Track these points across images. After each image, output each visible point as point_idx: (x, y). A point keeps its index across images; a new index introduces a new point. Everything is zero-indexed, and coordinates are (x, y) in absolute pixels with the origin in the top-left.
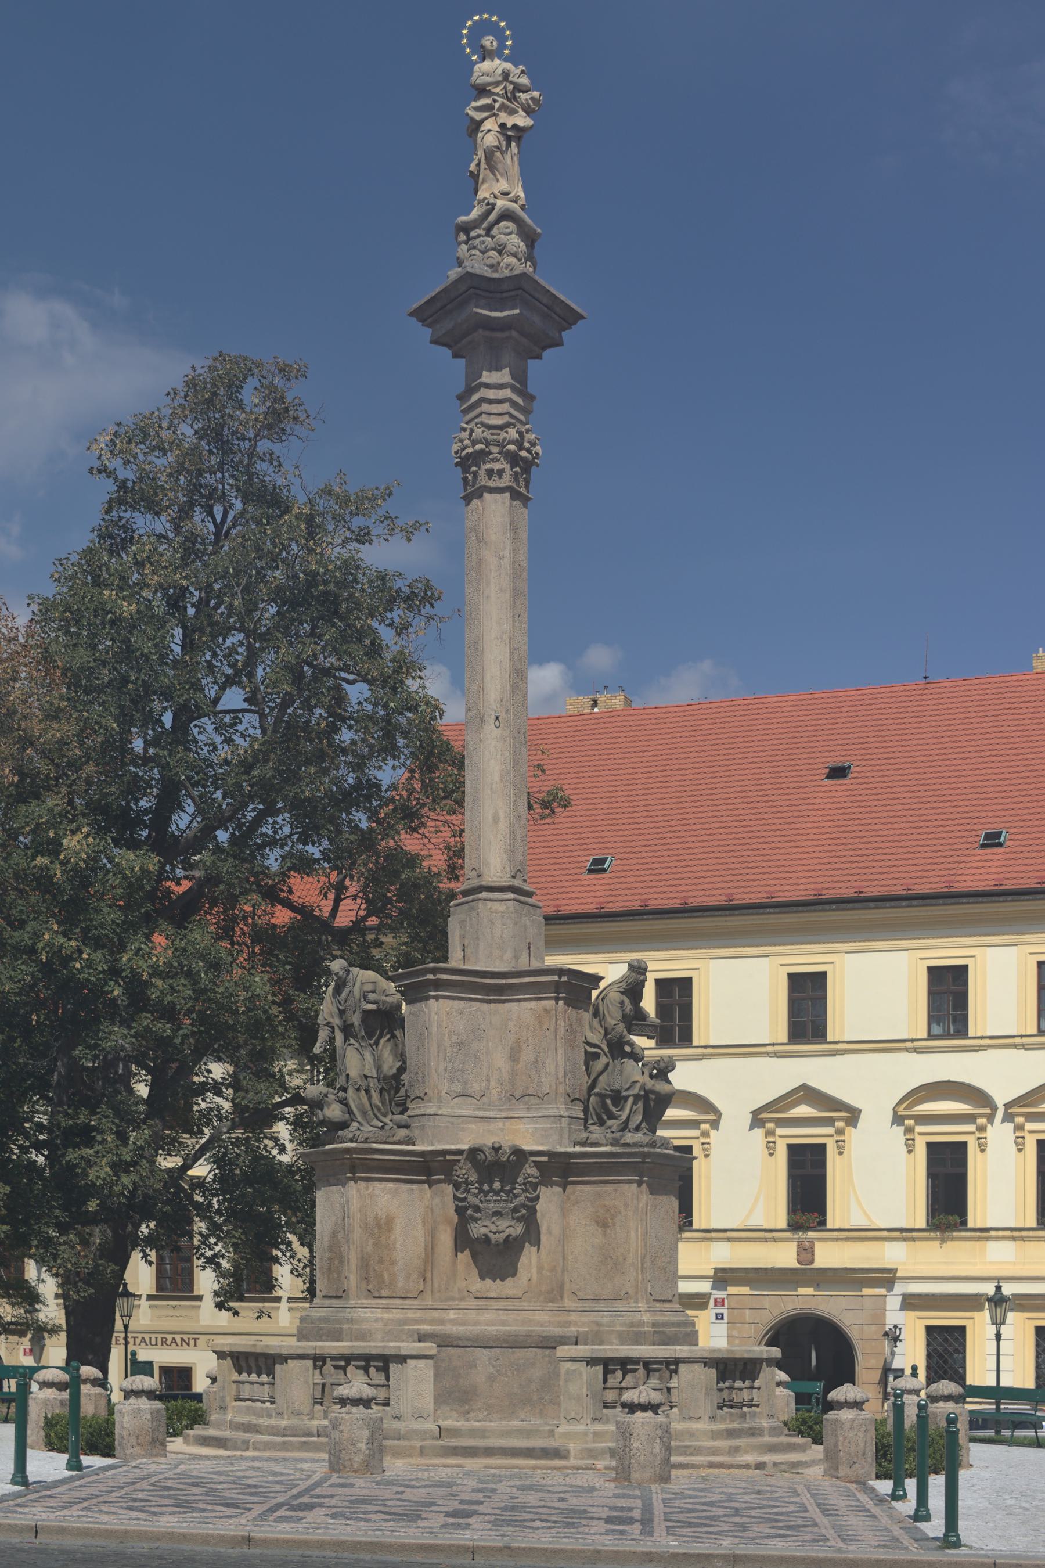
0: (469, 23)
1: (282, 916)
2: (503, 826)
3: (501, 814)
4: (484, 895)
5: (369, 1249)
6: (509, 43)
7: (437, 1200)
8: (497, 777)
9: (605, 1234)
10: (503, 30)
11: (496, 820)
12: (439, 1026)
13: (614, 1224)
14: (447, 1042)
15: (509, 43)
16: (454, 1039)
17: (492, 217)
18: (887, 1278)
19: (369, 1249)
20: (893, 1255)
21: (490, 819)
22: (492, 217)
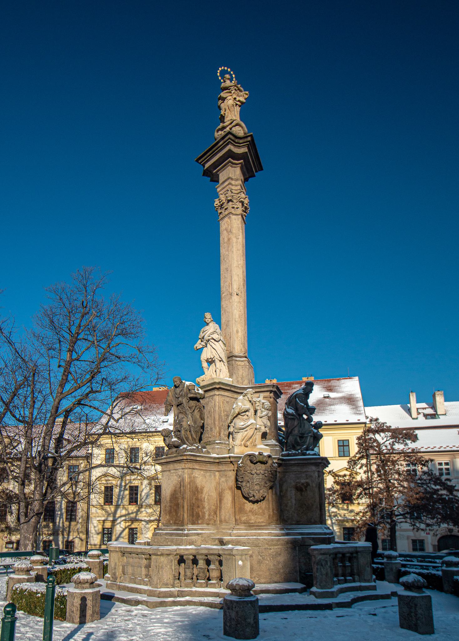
0: (218, 74)
1: (39, 595)
2: (240, 334)
3: (240, 330)
4: (234, 358)
5: (194, 501)
6: (229, 70)
7: (223, 479)
8: (237, 316)
9: (301, 495)
10: (230, 72)
11: (237, 332)
12: (219, 407)
13: (306, 490)
14: (223, 414)
15: (229, 70)
16: (225, 413)
17: (233, 124)
19: (194, 501)
21: (235, 332)
22: (233, 124)
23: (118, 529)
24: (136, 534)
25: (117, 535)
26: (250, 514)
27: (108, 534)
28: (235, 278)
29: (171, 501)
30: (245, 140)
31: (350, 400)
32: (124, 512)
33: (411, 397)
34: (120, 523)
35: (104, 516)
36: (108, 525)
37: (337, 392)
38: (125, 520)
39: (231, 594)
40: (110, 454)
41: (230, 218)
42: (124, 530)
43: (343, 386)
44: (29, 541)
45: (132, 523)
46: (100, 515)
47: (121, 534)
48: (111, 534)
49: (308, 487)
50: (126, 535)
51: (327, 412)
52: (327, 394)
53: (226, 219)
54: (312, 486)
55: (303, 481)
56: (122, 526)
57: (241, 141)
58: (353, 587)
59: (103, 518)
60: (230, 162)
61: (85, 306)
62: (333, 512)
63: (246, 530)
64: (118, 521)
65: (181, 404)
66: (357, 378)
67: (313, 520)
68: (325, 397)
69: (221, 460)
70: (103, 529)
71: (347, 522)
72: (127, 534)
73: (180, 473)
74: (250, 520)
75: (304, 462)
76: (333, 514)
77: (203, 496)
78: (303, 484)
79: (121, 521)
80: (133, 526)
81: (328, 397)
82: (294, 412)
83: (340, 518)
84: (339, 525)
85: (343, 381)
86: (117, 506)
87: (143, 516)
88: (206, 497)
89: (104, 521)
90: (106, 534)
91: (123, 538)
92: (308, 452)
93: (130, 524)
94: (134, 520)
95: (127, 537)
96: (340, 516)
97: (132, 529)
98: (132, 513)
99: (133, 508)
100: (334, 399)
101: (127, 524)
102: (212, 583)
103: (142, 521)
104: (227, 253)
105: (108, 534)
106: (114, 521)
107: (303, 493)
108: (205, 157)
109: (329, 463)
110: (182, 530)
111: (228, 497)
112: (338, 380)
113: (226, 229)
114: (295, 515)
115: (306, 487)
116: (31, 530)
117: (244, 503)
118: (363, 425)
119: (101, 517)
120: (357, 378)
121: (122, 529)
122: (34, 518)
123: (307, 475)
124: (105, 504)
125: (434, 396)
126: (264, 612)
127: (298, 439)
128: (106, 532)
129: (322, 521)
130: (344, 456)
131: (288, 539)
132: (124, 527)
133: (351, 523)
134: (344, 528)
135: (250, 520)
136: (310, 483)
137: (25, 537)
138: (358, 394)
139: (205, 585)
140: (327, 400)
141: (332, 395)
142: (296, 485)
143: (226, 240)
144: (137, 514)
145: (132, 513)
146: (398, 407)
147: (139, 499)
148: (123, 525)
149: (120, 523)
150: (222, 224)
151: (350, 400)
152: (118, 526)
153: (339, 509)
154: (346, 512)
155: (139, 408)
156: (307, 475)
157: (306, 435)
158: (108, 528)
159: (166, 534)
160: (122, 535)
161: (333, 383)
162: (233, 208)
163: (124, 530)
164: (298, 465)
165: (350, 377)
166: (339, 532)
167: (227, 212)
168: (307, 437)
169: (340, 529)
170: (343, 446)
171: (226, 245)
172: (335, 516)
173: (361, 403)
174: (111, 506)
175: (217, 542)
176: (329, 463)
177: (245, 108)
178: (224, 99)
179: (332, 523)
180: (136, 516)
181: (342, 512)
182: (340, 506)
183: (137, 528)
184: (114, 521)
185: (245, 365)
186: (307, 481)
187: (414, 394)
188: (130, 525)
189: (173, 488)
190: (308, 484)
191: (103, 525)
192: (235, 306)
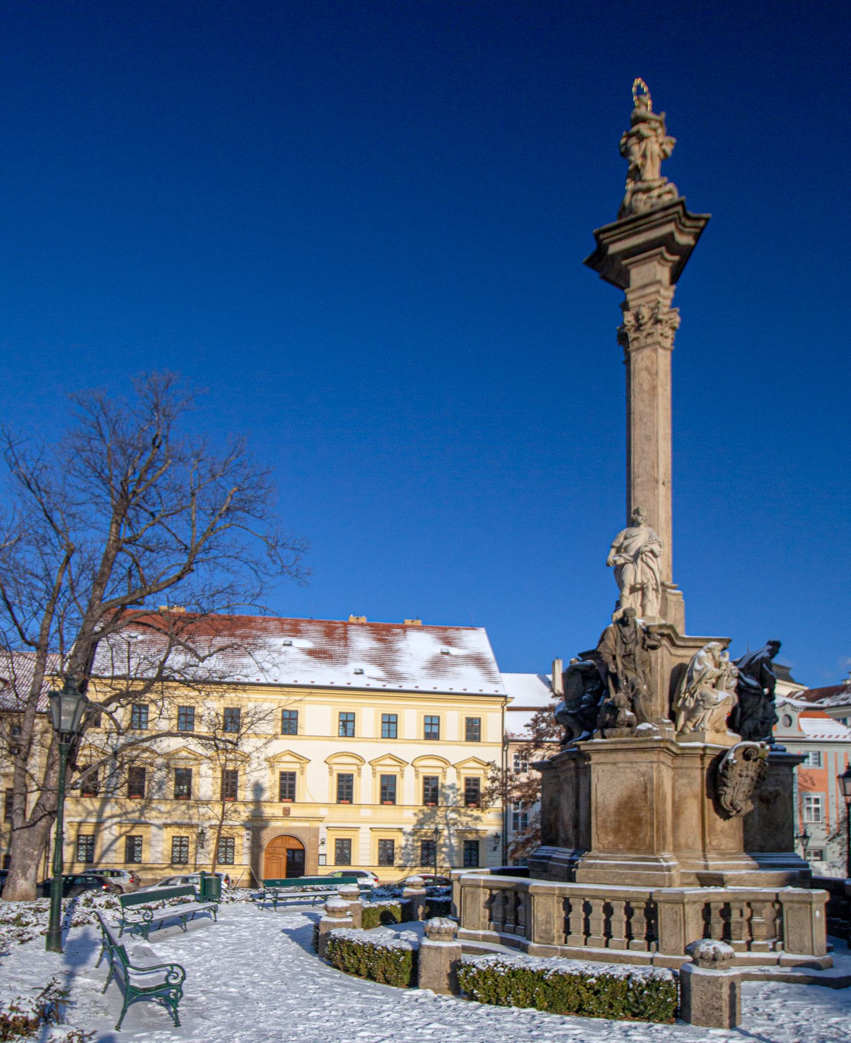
9: (768, 809)
18: (321, 819)
20: (323, 812)
23: (106, 836)
24: (140, 845)
25: (105, 847)
26: (721, 835)
27: (87, 844)
28: (661, 455)
29: (618, 811)
30: (695, 223)
31: (478, 661)
32: (117, 810)
33: (556, 665)
34: (110, 827)
35: (80, 815)
36: (88, 830)
37: (459, 647)
38: (120, 823)
40: (187, 717)
41: (656, 351)
42: (117, 839)
43: (465, 639)
44: (32, 859)
45: (133, 828)
46: (73, 813)
47: (111, 845)
48: (92, 844)
50: (120, 847)
51: (449, 675)
52: (445, 648)
53: (647, 352)
55: (771, 789)
56: (113, 832)
57: (688, 223)
59: (78, 819)
60: (661, 254)
61: (157, 443)
62: (452, 819)
63: (722, 860)
64: (107, 824)
65: (630, 655)
66: (482, 631)
67: (783, 846)
68: (443, 653)
69: (687, 751)
70: (78, 836)
71: (471, 833)
72: (124, 845)
73: (643, 768)
74: (721, 844)
75: (778, 761)
76: (451, 822)
78: (770, 793)
79: (112, 825)
80: (134, 833)
81: (447, 654)
83: (460, 827)
84: (459, 837)
85: (464, 632)
86: (105, 801)
87: (151, 816)
89: (80, 824)
90: (82, 844)
91: (115, 851)
93: (128, 829)
94: (136, 824)
95: (123, 849)
96: (462, 824)
97: (131, 839)
98: (133, 812)
99: (131, 805)
100: (456, 657)
101: (124, 830)
102: (759, 945)
103: (151, 824)
104: (648, 410)
105: (87, 844)
106: (99, 824)
107: (771, 806)
108: (613, 233)
110: (657, 860)
111: (692, 810)
112: (458, 629)
113: (647, 369)
114: (759, 837)
115: (776, 797)
116: (37, 840)
117: (716, 819)
118: (503, 699)
119: (73, 816)
120: (482, 631)
121: (113, 838)
122: (44, 820)
123: (777, 780)
124: (82, 796)
125: (554, 663)
126: (823, 985)
127: (759, 726)
128: (81, 841)
129: (791, 848)
130: (389, 738)
131: (780, 874)
132: (117, 834)
133: (474, 835)
134: (466, 842)
135: (721, 844)
136: (781, 792)
137: (24, 853)
138: (487, 651)
139: (746, 947)
140: (446, 657)
141: (453, 651)
143: (646, 387)
144: (142, 814)
145: (133, 812)
146: (534, 677)
147: (146, 789)
148: (116, 830)
149: (110, 827)
150: (639, 360)
151: (478, 661)
152: (106, 832)
153: (460, 815)
154: (469, 819)
155: (140, 638)
156: (777, 780)
158: (87, 836)
159: (617, 866)
160: (114, 848)
161: (451, 633)
162: (662, 335)
163: (117, 839)
165: (473, 627)
166: (459, 846)
167: (649, 340)
169: (460, 842)
170: (389, 723)
171: (646, 396)
172: (454, 824)
173: (494, 667)
174: (94, 800)
175: (692, 879)
177: (668, 167)
178: (641, 138)
179: (450, 834)
180: (140, 817)
181: (465, 819)
182: (463, 810)
183: (141, 836)
184: (99, 824)
185: (678, 601)
186: (777, 788)
187: (561, 662)
188: (129, 832)
189: (626, 793)
191: (78, 831)
192: (657, 500)
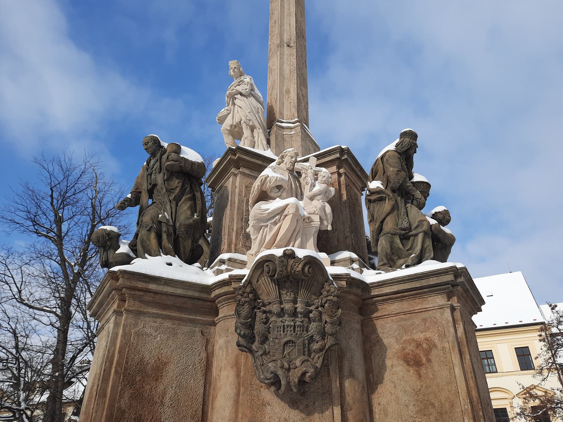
13: (429, 361)
39: (352, 375)
49: (434, 352)
54: (444, 348)
58: (330, 155)
77: (161, 387)
82: (382, 187)
88: (170, 393)
92: (277, 287)
107: (423, 371)
109: (483, 302)
115: (428, 353)
127: (397, 240)
142: (404, 349)
157: (414, 232)
164: (399, 296)
168: (416, 235)
176: (483, 302)
186: (428, 335)
190: (432, 346)
